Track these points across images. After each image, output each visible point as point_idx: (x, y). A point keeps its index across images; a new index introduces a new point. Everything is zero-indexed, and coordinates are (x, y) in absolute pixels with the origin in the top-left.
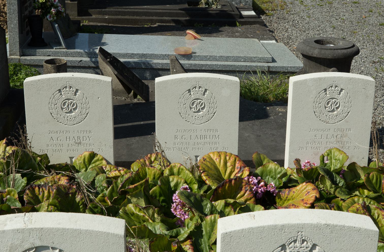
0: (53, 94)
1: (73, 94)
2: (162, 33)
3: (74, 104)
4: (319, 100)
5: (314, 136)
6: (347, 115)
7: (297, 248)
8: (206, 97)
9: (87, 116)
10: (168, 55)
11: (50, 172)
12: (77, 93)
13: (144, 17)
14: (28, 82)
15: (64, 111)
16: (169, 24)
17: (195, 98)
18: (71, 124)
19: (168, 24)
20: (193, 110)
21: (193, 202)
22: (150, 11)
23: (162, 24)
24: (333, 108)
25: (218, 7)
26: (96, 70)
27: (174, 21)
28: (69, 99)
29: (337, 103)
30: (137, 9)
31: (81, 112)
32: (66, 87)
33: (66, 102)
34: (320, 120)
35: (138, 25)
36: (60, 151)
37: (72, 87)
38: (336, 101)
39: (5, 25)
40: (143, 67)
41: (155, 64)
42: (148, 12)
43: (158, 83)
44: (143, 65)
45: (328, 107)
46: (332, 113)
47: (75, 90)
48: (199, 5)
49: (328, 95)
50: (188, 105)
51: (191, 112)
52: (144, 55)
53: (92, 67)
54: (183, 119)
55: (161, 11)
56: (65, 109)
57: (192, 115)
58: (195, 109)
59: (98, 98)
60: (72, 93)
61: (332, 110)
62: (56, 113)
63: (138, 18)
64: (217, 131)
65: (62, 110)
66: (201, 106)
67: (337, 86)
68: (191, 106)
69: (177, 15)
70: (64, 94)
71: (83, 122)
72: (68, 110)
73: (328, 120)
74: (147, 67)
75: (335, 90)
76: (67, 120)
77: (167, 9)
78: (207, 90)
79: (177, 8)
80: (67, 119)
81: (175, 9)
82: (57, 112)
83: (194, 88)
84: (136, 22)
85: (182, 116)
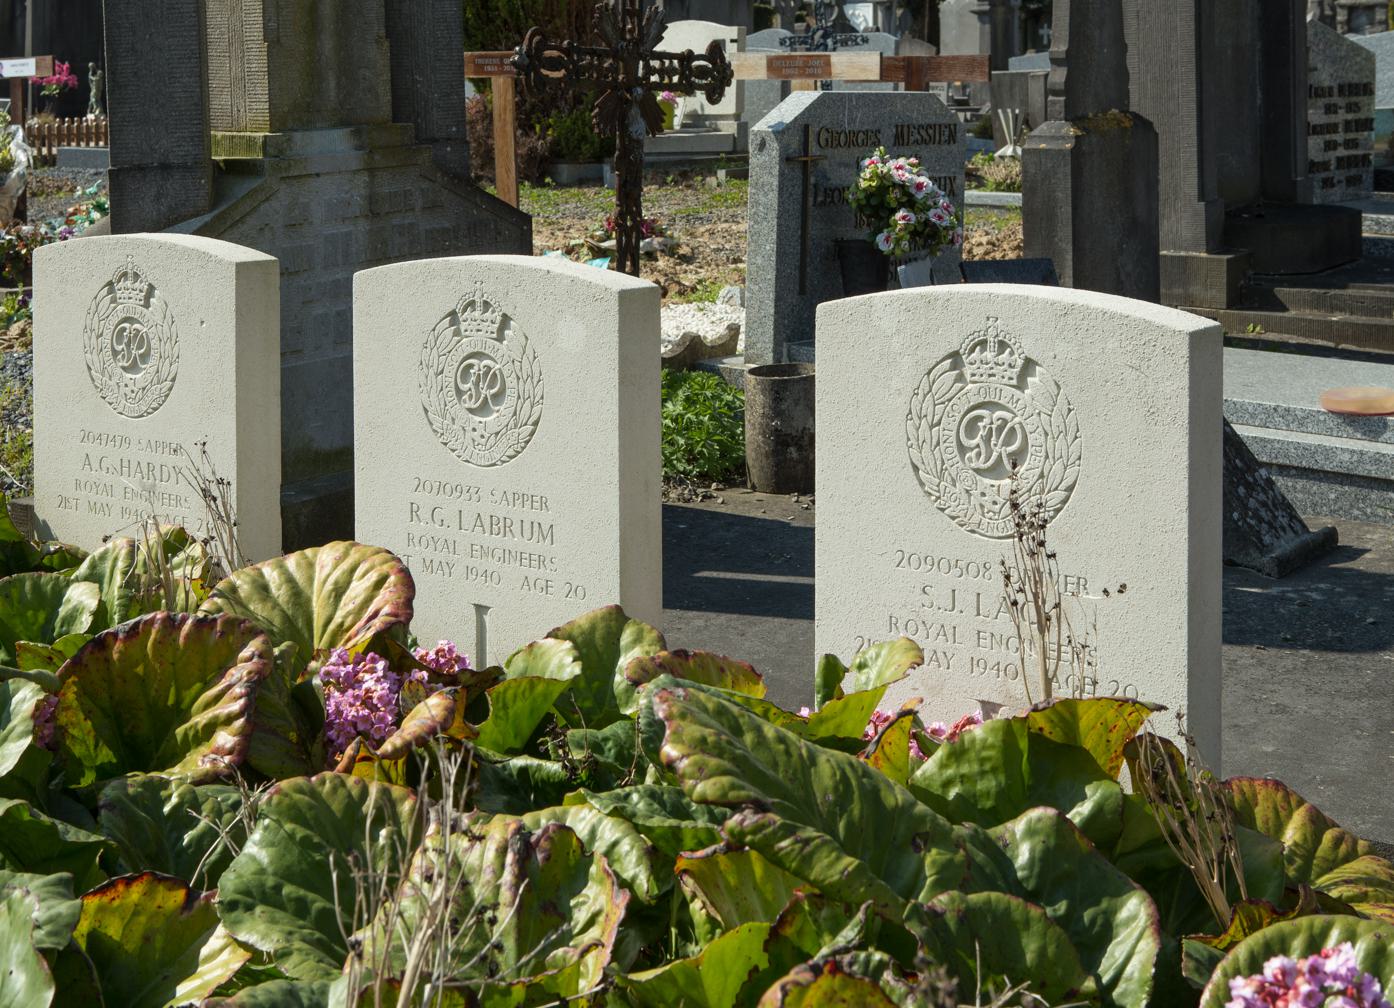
0: (929, 373)
1: (1011, 379)
5: (918, 591)
6: (1065, 502)
7: (987, 364)
9: (1068, 498)
12: (1029, 379)
15: (970, 460)
17: (981, 400)
18: (996, 534)
21: (339, 815)
28: (992, 406)
31: (515, 414)
32: (983, 344)
33: (980, 418)
37: (1009, 346)
46: (993, 482)
47: (1020, 362)
51: (459, 410)
54: (926, 498)
59: (202, 322)
60: (1008, 374)
64: (544, 504)
68: (459, 380)
70: (973, 375)
72: (987, 459)
73: (977, 517)
75: (997, 364)
76: (978, 507)
80: (982, 506)
82: (939, 463)
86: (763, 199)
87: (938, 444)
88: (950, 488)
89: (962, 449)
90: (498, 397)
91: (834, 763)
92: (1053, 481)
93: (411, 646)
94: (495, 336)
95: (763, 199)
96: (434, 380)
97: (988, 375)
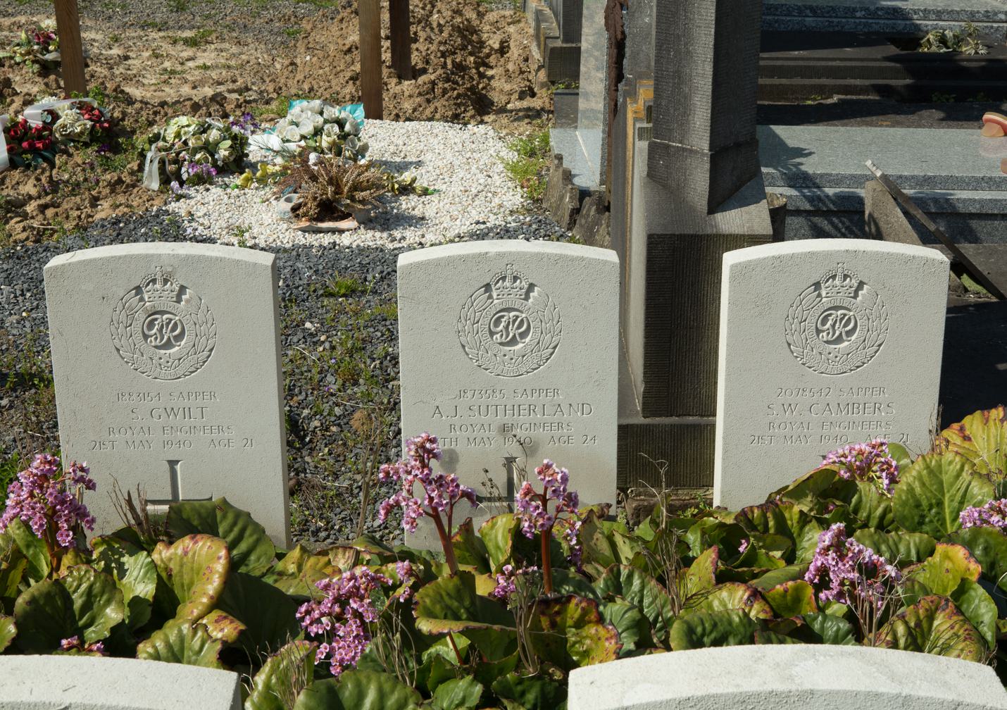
0: (122, 299)
2: (863, 119)
4: (473, 315)
6: (876, 352)
8: (531, 304)
9: (553, 352)
10: (990, 178)
12: (183, 297)
13: (798, 81)
14: (51, 267)
15: (151, 341)
16: (865, 97)
18: (169, 378)
19: (861, 97)
20: (823, 337)
22: (812, 63)
23: (849, 97)
24: (837, 333)
25: (980, 52)
26: (812, 218)
27: (878, 89)
28: (162, 313)
30: (778, 59)
32: (154, 281)
33: (156, 319)
34: (804, 364)
35: (787, 99)
36: (146, 445)
39: (468, 106)
40: (933, 211)
41: (965, 201)
42: (809, 67)
43: (403, 267)
44: (932, 205)
45: (824, 331)
46: (510, 348)
48: (921, 46)
49: (824, 300)
50: (810, 325)
51: (148, 348)
52: (928, 180)
53: (805, 211)
55: (837, 63)
56: (153, 338)
57: (819, 350)
58: (828, 334)
61: (511, 340)
62: (129, 348)
63: (784, 81)
65: (818, 336)
66: (519, 327)
67: (848, 276)
69: (881, 73)
72: (833, 336)
73: (501, 367)
74: (943, 209)
77: (850, 60)
78: (865, 284)
79: (879, 56)
80: (160, 365)
82: (132, 346)
83: (831, 280)
84: (781, 92)
85: (123, 358)
87: (131, 336)
88: (140, 358)
89: (146, 337)
90: (179, 337)
92: (200, 348)
94: (174, 299)
96: (125, 319)
97: (156, 296)
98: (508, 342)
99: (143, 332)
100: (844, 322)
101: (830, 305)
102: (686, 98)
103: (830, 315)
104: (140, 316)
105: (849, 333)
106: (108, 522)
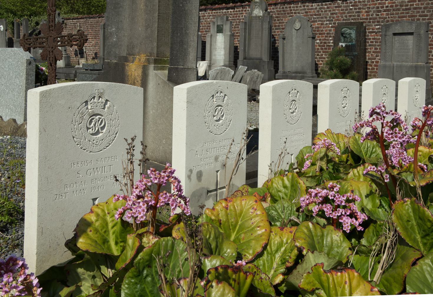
0: (78, 109)
1: (102, 106)
3: (102, 121)
6: (115, 138)
7: (95, 103)
11: (347, 150)
18: (97, 151)
24: (97, 129)
29: (102, 120)
38: (100, 118)
45: (90, 128)
46: (95, 136)
59: (69, 108)
65: (88, 131)
66: (100, 124)
70: (92, 107)
71: (111, 146)
75: (98, 103)
81: (401, 32)
83: (93, 99)
86: (30, 78)
91: (398, 215)
93: (188, 202)
95: (30, 78)
96: (79, 119)
98: (95, 133)
99: (87, 126)
100: (99, 122)
101: (217, 105)
102: (185, 50)
103: (93, 119)
104: (86, 117)
105: (103, 128)
106: (59, 245)
